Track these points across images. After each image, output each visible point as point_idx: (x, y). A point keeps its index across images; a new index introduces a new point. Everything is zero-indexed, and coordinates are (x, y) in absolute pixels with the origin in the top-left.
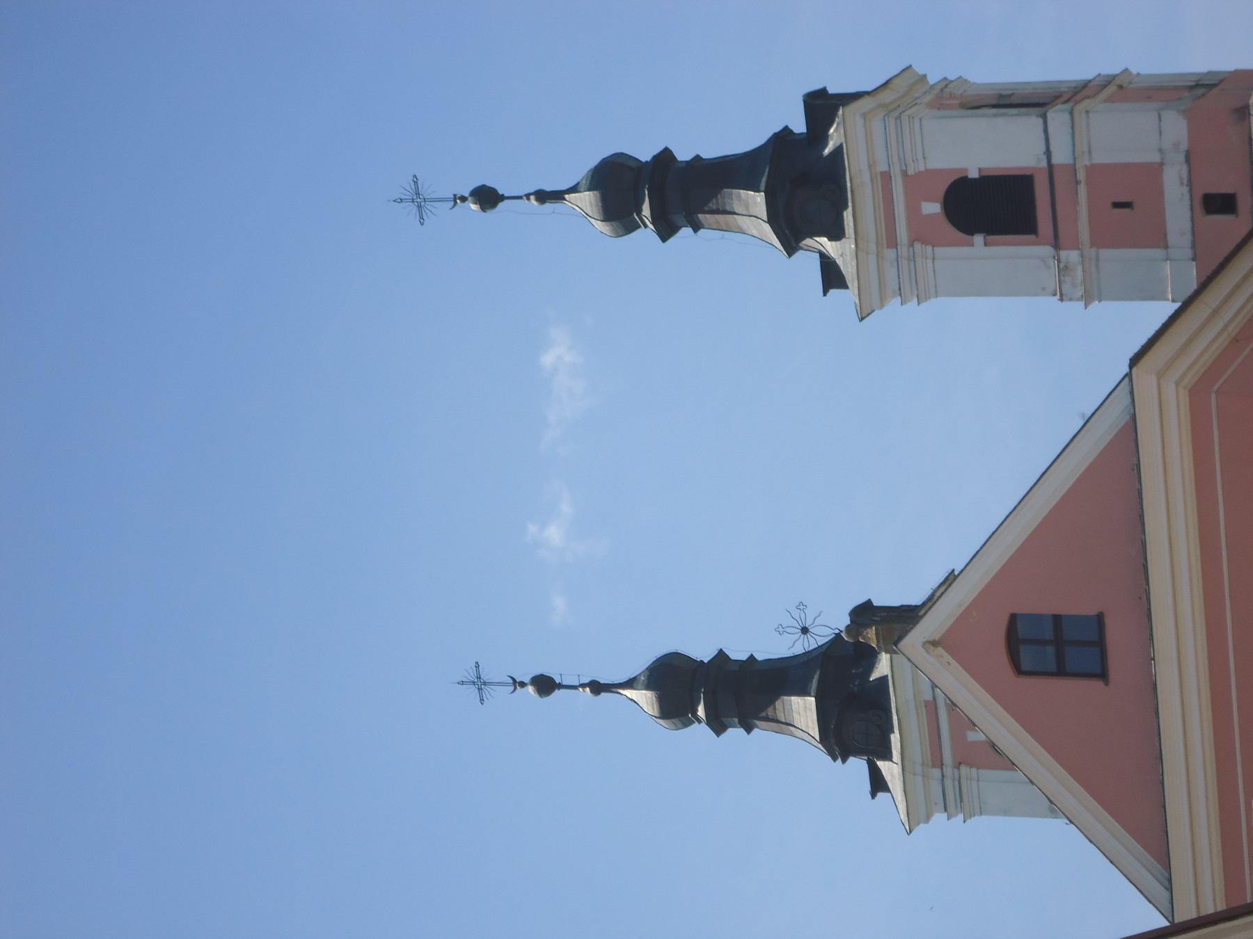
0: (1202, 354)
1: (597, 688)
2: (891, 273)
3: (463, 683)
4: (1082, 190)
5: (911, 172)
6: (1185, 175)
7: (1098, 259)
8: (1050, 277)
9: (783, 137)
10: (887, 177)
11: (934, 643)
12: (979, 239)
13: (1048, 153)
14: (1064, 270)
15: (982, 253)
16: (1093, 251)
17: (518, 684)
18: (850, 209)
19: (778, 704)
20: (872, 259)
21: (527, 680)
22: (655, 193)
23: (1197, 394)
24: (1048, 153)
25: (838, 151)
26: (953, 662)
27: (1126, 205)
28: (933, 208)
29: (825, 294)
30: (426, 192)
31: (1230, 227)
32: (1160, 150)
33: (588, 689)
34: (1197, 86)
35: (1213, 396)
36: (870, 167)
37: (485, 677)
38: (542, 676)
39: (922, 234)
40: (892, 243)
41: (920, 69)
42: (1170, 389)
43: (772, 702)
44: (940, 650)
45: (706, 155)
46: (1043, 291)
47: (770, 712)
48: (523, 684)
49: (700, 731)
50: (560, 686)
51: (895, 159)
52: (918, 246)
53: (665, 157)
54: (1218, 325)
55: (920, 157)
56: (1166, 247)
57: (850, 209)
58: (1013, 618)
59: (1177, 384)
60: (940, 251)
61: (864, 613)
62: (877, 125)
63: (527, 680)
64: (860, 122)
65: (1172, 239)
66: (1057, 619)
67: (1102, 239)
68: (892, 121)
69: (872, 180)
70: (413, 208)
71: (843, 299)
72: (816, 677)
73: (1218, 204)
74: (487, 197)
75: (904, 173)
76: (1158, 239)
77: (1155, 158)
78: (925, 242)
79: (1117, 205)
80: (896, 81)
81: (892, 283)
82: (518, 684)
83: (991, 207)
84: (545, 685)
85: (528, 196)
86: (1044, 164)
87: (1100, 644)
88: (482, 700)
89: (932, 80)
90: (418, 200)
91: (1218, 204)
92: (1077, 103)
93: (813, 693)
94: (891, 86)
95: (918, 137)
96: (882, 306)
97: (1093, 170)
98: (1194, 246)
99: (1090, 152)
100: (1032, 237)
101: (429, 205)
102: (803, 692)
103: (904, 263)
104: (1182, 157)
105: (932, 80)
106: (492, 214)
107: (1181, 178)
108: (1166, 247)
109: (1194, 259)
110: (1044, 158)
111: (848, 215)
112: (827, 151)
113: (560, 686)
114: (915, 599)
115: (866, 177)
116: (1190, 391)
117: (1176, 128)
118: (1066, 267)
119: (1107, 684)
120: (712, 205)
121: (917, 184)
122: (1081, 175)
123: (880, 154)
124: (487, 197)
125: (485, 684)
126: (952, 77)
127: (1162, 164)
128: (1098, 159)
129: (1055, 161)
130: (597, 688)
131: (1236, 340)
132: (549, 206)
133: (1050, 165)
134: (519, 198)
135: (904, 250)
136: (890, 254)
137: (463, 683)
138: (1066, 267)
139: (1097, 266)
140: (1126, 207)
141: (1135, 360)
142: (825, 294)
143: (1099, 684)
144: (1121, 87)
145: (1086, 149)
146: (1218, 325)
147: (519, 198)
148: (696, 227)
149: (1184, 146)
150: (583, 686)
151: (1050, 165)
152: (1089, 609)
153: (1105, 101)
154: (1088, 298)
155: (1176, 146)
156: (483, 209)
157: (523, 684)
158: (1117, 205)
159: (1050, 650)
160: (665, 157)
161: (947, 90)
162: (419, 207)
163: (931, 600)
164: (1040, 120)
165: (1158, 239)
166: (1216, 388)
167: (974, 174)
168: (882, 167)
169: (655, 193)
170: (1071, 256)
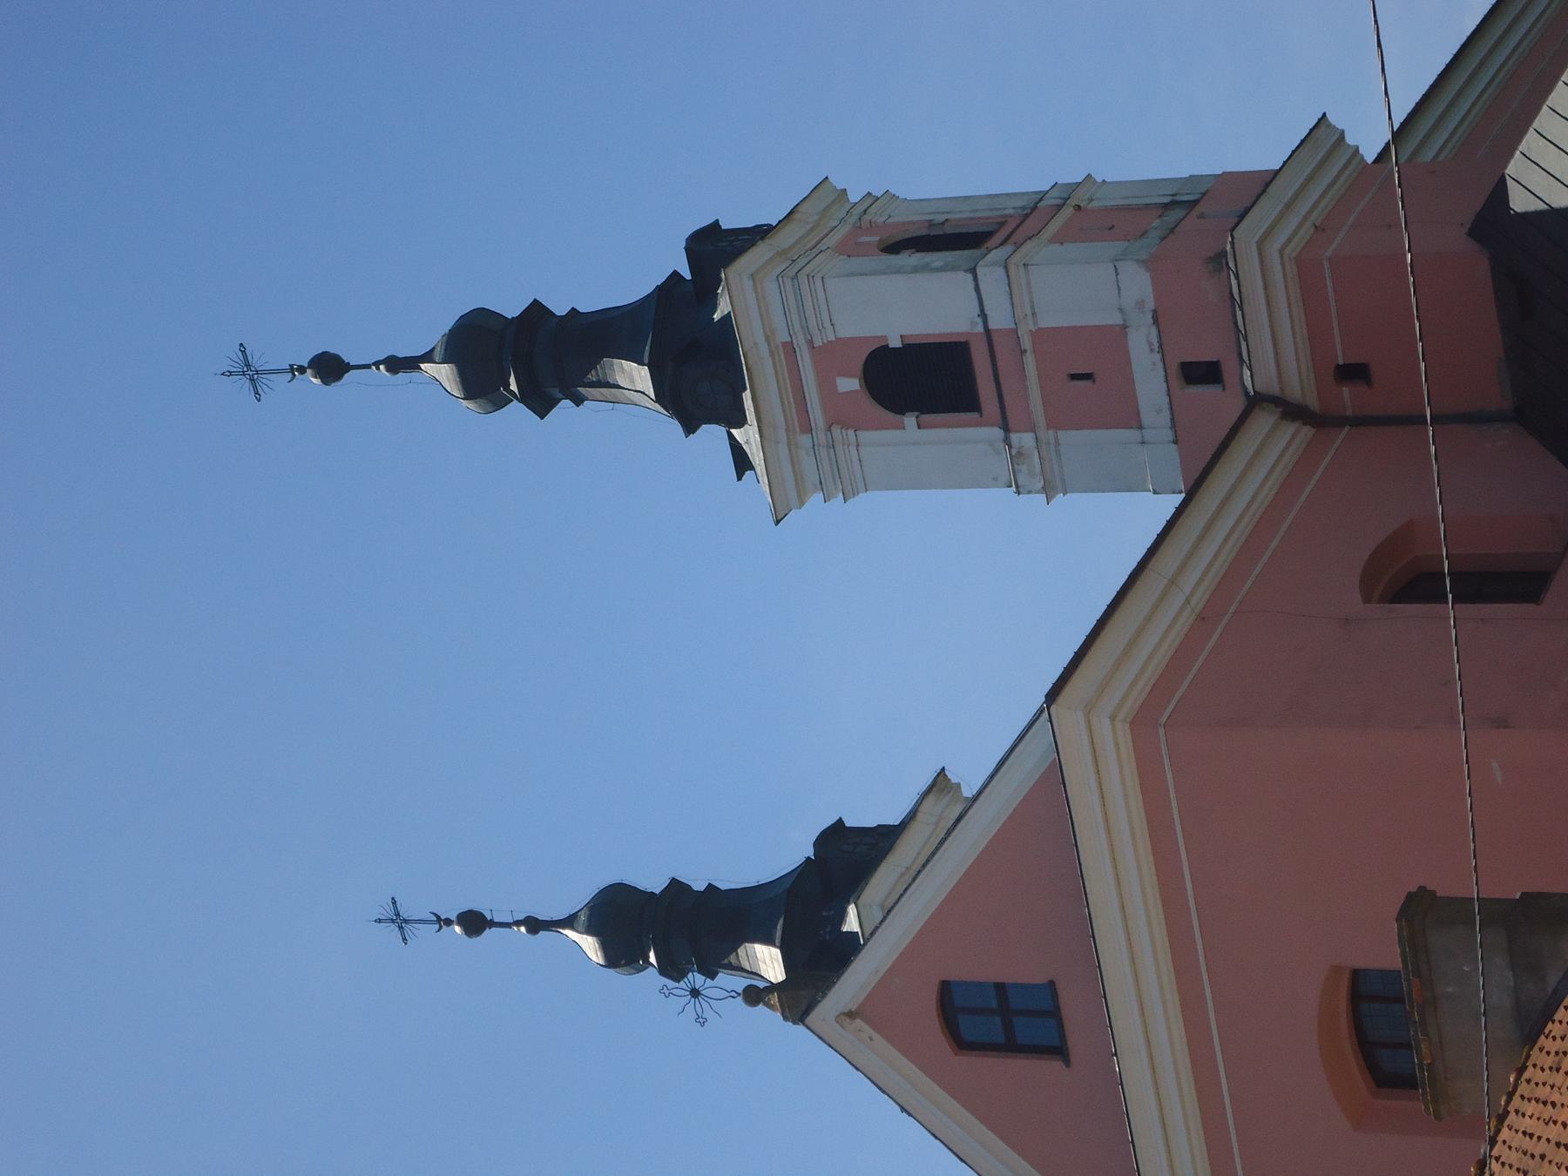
0: (1150, 657)
1: (534, 925)
2: (808, 463)
3: (379, 921)
4: (1030, 361)
5: (818, 342)
6: (1155, 341)
7: (1057, 444)
8: (1000, 464)
10: (790, 348)
11: (851, 1015)
12: (910, 420)
13: (983, 315)
14: (1017, 457)
15: (912, 439)
16: (1051, 433)
18: (748, 391)
19: (741, 951)
20: (783, 450)
21: (453, 918)
22: (523, 357)
23: (1142, 722)
24: (983, 315)
25: (727, 318)
26: (877, 1037)
27: (1088, 377)
28: (850, 384)
29: (739, 478)
30: (257, 363)
31: (1222, 403)
32: (1120, 309)
33: (523, 929)
34: (1172, 204)
35: (1161, 730)
36: (767, 339)
37: (404, 914)
38: (470, 912)
39: (841, 417)
40: (807, 428)
41: (838, 182)
42: (1103, 727)
43: (734, 949)
44: (859, 1022)
45: (585, 307)
46: (995, 482)
47: (732, 958)
48: (448, 922)
49: (651, 977)
50: (492, 924)
51: (797, 328)
52: (836, 431)
53: (536, 310)
54: (1177, 600)
55: (827, 324)
56: (1140, 427)
57: (748, 391)
58: (945, 988)
59: (1113, 718)
60: (866, 436)
61: (835, 837)
62: (771, 288)
63: (453, 918)
64: (748, 284)
65: (1147, 417)
66: (1000, 988)
67: (1057, 422)
68: (788, 282)
69: (772, 354)
70: (245, 381)
71: (758, 482)
72: (781, 922)
73: (1201, 373)
74: (330, 367)
75: (810, 343)
76: (1130, 418)
77: (1115, 319)
78: (845, 425)
79: (1074, 377)
80: (802, 208)
81: (811, 475)
83: (922, 382)
84: (474, 923)
85: (377, 364)
86: (980, 329)
87: (1054, 1013)
88: (404, 939)
89: (854, 197)
90: (250, 372)
91: (1201, 373)
92: (1018, 246)
93: (778, 941)
94: (796, 216)
95: (823, 306)
96: (801, 504)
97: (1039, 335)
98: (1174, 426)
99: (1034, 314)
100: (974, 416)
101: (264, 379)
102: (768, 941)
103: (823, 453)
104: (1149, 316)
105: (854, 197)
106: (335, 387)
107: (1150, 344)
108: (1140, 427)
109: (1175, 442)
110: (979, 321)
111: (747, 396)
112: (716, 316)
113: (492, 924)
114: (894, 819)
115: (764, 349)
116: (1131, 723)
117: (1138, 284)
118: (1019, 454)
119: (1068, 1063)
120: (592, 377)
121: (829, 356)
122: (1027, 343)
124: (330, 367)
125: (406, 921)
126: (877, 192)
127: (1124, 327)
128: (1045, 322)
129: (992, 326)
130: (534, 925)
131: (1201, 618)
132: (402, 376)
133: (988, 331)
134: (367, 366)
135: (821, 436)
136: (805, 440)
137: (379, 921)
138: (1019, 454)
139: (1058, 452)
140: (1086, 382)
141: (1052, 695)
142: (739, 478)
143: (1056, 1065)
144: (1078, 208)
145: (1029, 312)
146: (1177, 600)
147: (367, 366)
148: (578, 400)
149: (1150, 304)
150: (518, 923)
151: (988, 331)
152: (1040, 978)
153: (1053, 240)
154: (1049, 491)
155: (1140, 304)
156: (326, 382)
157: (448, 922)
158: (1074, 377)
159: (998, 1020)
160: (536, 310)
161: (867, 217)
162: (252, 380)
163: (912, 815)
164: (969, 277)
165: (1130, 418)
166: (1163, 720)
167: (895, 343)
169: (523, 357)
170: (1023, 439)
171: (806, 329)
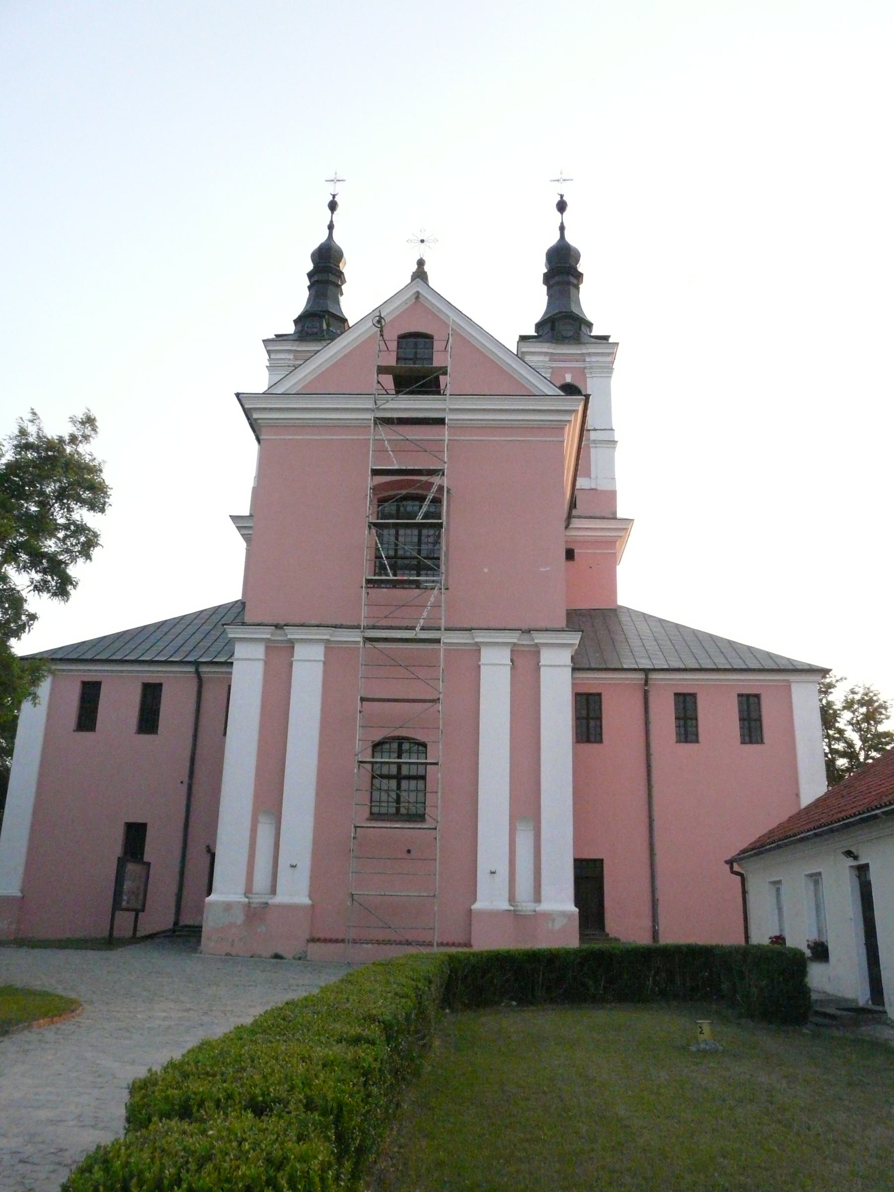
9: (590, 325)
17: (334, 196)
22: (562, 268)
28: (568, 379)
50: (332, 213)
52: (550, 370)
58: (428, 337)
75: (585, 368)
82: (334, 196)
123: (594, 359)
168: (588, 359)
171: (591, 368)
